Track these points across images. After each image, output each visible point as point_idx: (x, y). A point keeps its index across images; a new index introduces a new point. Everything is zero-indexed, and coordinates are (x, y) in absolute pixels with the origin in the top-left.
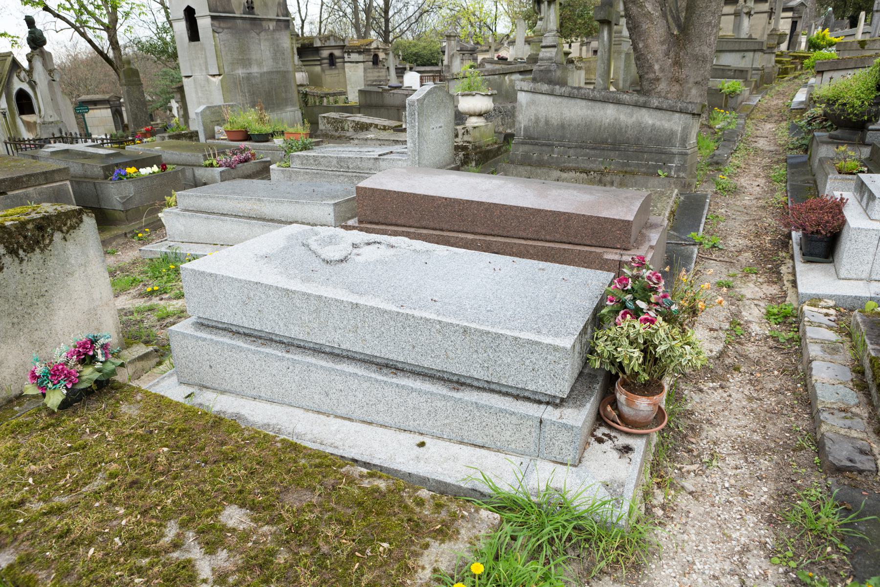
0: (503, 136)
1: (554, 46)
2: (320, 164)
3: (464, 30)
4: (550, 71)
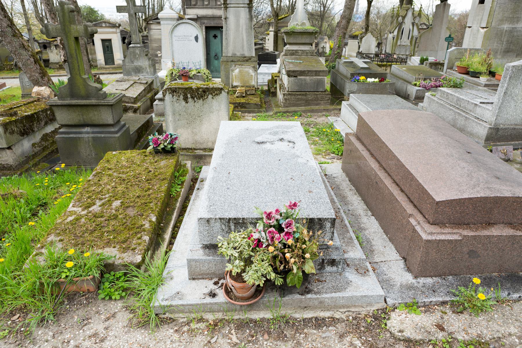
2: (448, 99)
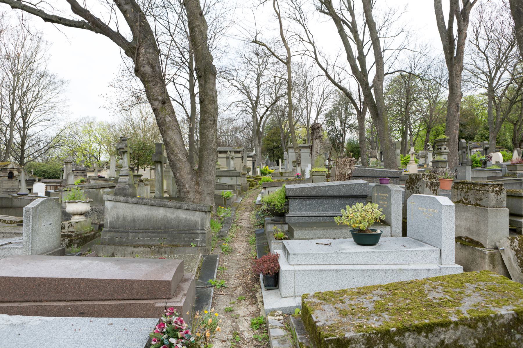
0: (98, 226)
1: (127, 176)
3: (79, 158)
4: (125, 189)
